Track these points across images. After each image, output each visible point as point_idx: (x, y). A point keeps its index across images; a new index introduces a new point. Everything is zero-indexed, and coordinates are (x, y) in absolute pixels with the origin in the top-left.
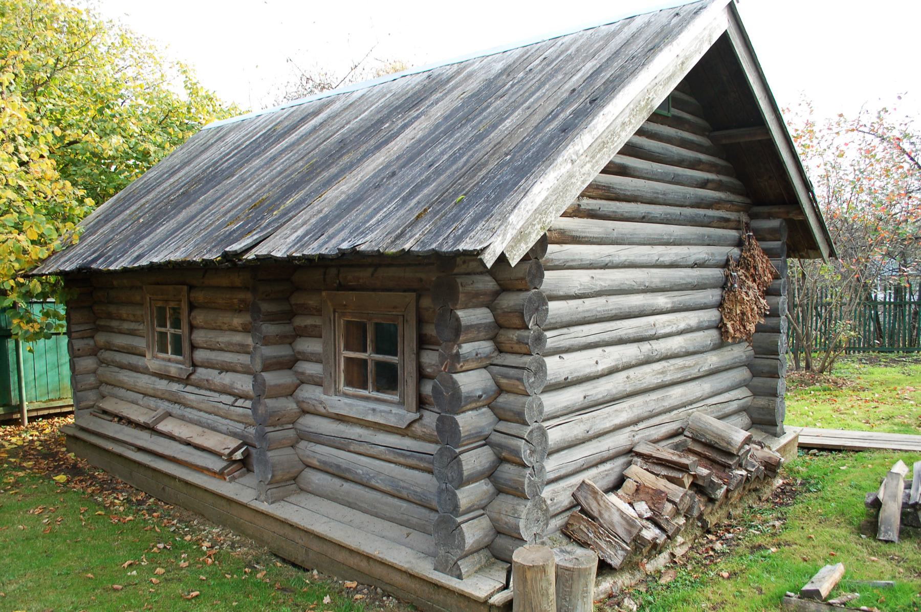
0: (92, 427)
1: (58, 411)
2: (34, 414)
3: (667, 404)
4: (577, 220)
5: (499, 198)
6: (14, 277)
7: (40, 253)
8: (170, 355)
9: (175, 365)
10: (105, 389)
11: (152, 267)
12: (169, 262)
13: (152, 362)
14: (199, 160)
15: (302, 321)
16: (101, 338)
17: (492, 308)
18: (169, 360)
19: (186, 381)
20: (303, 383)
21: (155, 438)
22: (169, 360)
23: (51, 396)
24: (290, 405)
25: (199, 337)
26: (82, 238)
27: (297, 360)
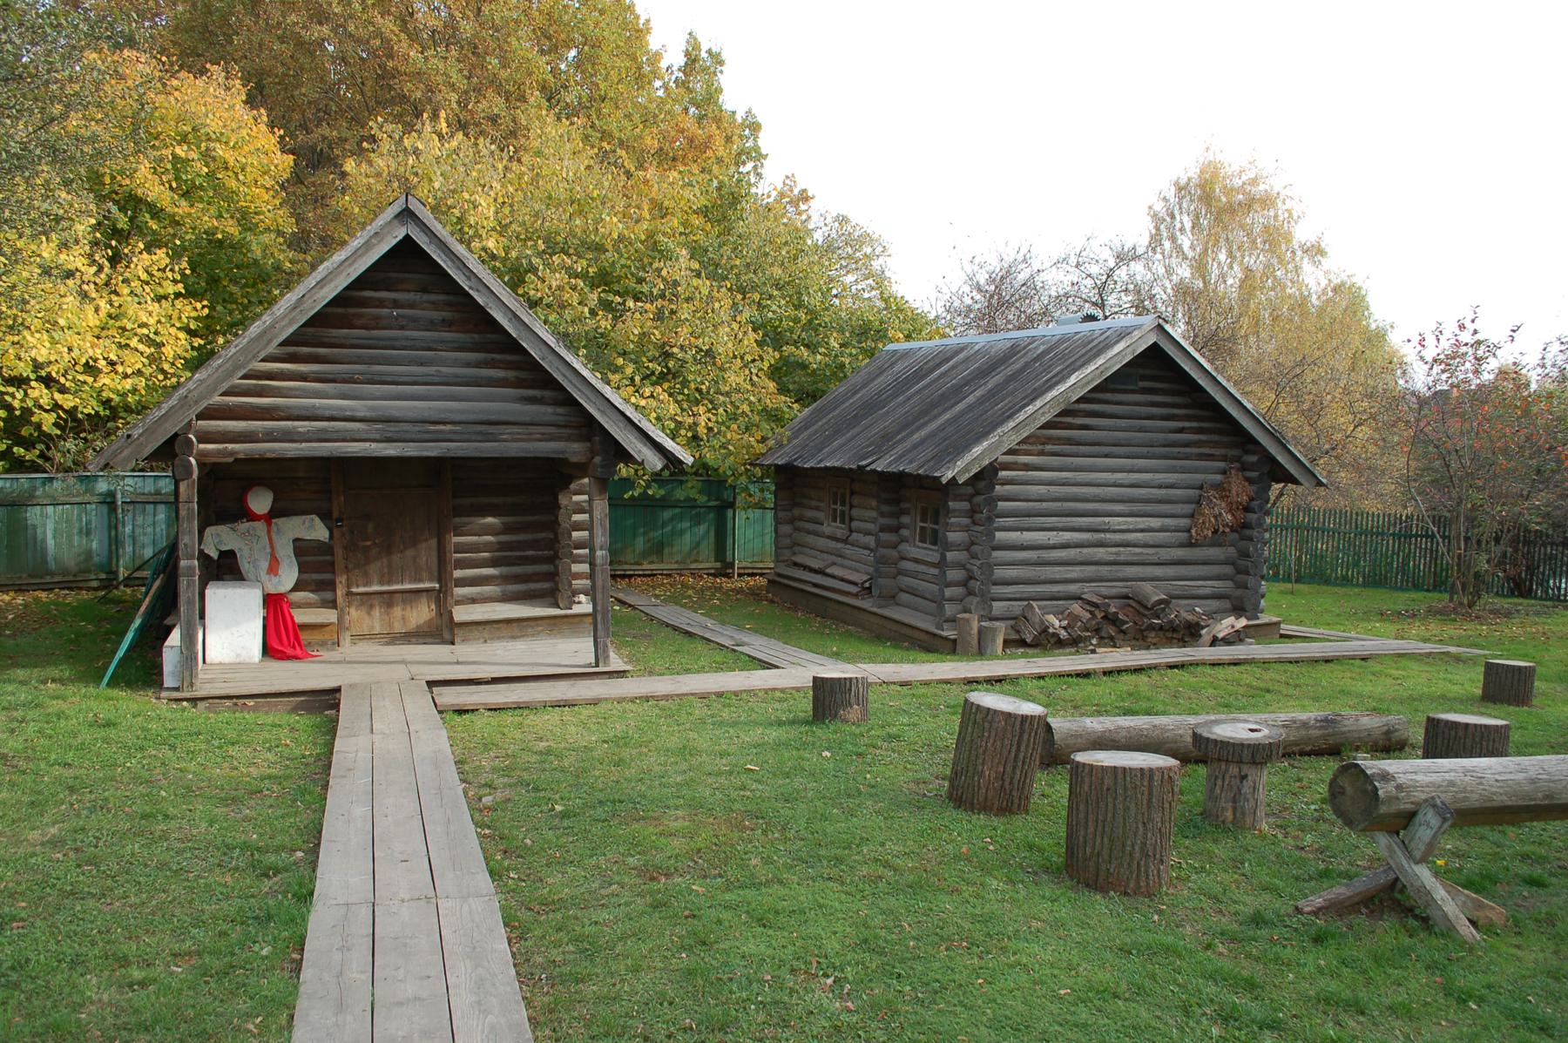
0: (785, 573)
1: (759, 571)
2: (742, 571)
3: (1120, 575)
4: (1042, 457)
5: (963, 451)
6: (745, 464)
7: (761, 448)
8: (838, 524)
9: (838, 529)
10: (797, 549)
11: (826, 468)
12: (834, 467)
13: (827, 529)
14: (876, 382)
15: (904, 505)
16: (797, 511)
17: (970, 502)
18: (837, 527)
19: (845, 541)
20: (902, 541)
21: (824, 578)
22: (837, 527)
23: (755, 559)
24: (894, 554)
25: (855, 512)
26: (790, 440)
27: (900, 528)
